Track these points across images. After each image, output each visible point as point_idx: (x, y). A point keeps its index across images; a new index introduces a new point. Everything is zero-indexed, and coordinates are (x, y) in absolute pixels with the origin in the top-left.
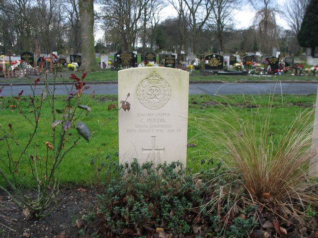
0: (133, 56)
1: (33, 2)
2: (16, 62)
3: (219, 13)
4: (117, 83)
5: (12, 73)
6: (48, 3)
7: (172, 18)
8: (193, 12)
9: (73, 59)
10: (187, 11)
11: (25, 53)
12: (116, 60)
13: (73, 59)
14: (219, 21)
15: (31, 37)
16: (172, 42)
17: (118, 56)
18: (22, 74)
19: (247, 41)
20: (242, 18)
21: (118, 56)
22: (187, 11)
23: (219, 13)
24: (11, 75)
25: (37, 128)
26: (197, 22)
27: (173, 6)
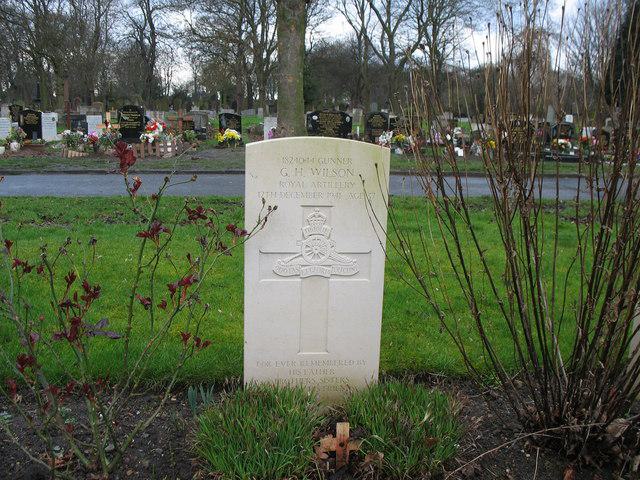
0: (344, 119)
1: (60, 3)
2: (156, 127)
3: (435, 33)
4: (244, 173)
5: (150, 148)
6: (89, 7)
7: (332, 42)
8: (389, 33)
9: (224, 123)
10: (375, 34)
11: (126, 109)
12: (310, 126)
13: (224, 123)
14: (434, 52)
15: (61, 70)
16: (342, 94)
17: (315, 118)
18: (169, 149)
19: (480, 90)
20: (477, 46)
21: (315, 118)
22: (375, 34)
23: (435, 33)
24: (147, 151)
25: (485, 254)
26: (397, 50)
27: (345, 20)
